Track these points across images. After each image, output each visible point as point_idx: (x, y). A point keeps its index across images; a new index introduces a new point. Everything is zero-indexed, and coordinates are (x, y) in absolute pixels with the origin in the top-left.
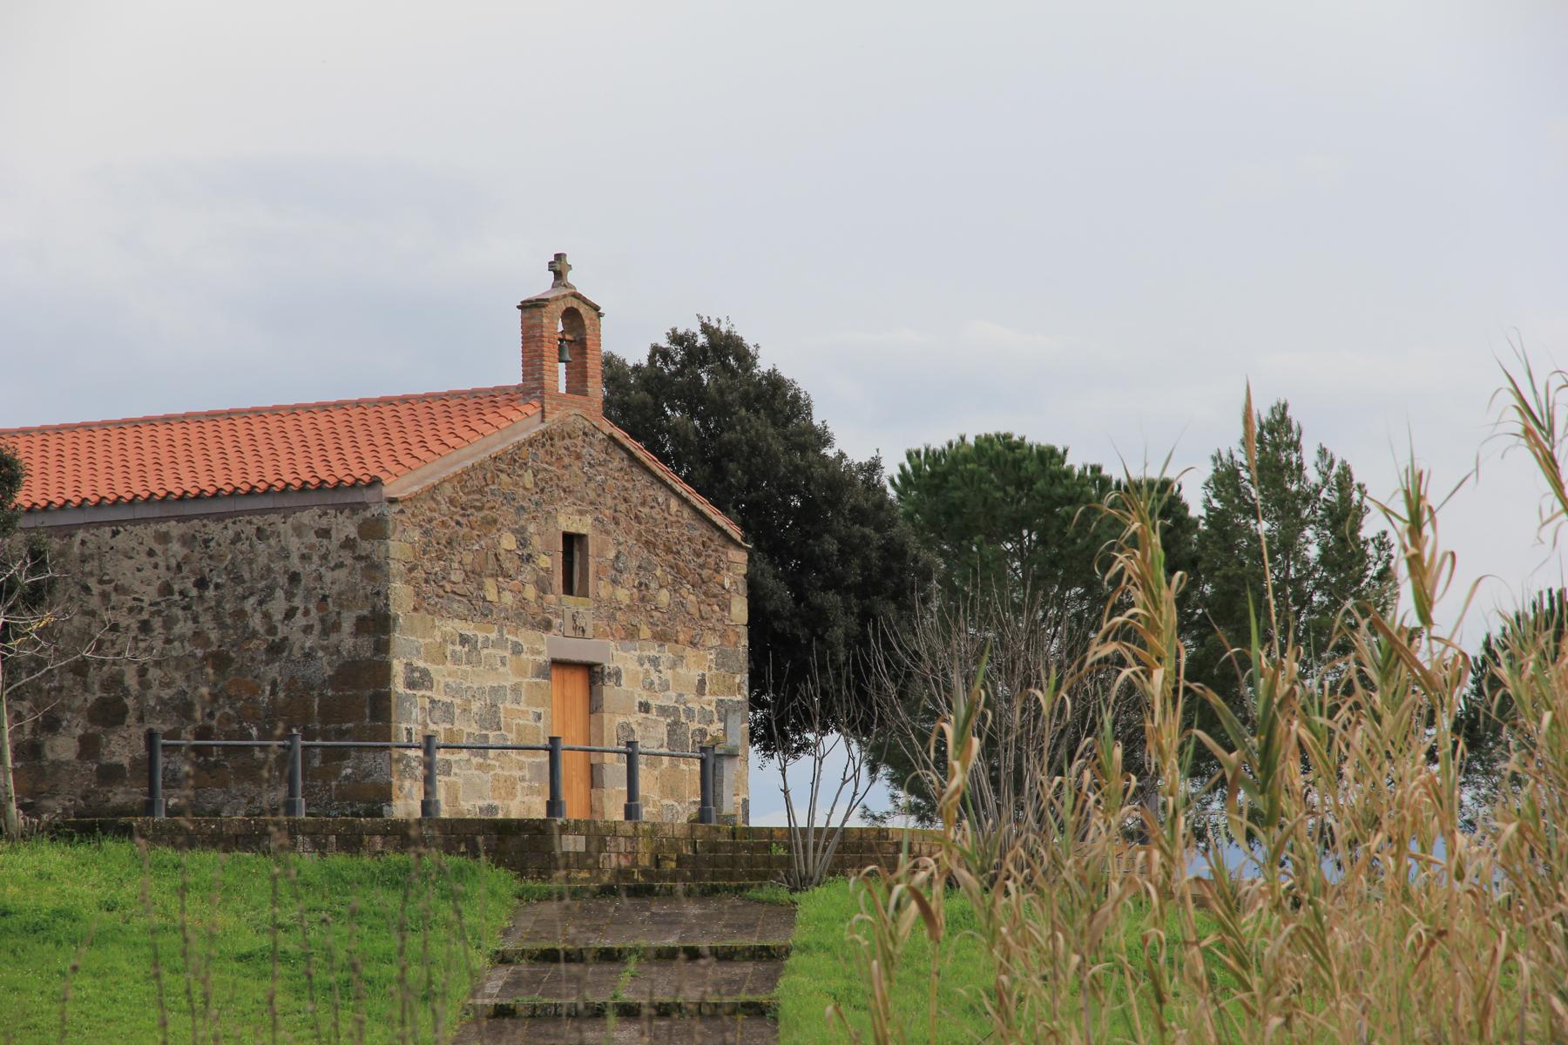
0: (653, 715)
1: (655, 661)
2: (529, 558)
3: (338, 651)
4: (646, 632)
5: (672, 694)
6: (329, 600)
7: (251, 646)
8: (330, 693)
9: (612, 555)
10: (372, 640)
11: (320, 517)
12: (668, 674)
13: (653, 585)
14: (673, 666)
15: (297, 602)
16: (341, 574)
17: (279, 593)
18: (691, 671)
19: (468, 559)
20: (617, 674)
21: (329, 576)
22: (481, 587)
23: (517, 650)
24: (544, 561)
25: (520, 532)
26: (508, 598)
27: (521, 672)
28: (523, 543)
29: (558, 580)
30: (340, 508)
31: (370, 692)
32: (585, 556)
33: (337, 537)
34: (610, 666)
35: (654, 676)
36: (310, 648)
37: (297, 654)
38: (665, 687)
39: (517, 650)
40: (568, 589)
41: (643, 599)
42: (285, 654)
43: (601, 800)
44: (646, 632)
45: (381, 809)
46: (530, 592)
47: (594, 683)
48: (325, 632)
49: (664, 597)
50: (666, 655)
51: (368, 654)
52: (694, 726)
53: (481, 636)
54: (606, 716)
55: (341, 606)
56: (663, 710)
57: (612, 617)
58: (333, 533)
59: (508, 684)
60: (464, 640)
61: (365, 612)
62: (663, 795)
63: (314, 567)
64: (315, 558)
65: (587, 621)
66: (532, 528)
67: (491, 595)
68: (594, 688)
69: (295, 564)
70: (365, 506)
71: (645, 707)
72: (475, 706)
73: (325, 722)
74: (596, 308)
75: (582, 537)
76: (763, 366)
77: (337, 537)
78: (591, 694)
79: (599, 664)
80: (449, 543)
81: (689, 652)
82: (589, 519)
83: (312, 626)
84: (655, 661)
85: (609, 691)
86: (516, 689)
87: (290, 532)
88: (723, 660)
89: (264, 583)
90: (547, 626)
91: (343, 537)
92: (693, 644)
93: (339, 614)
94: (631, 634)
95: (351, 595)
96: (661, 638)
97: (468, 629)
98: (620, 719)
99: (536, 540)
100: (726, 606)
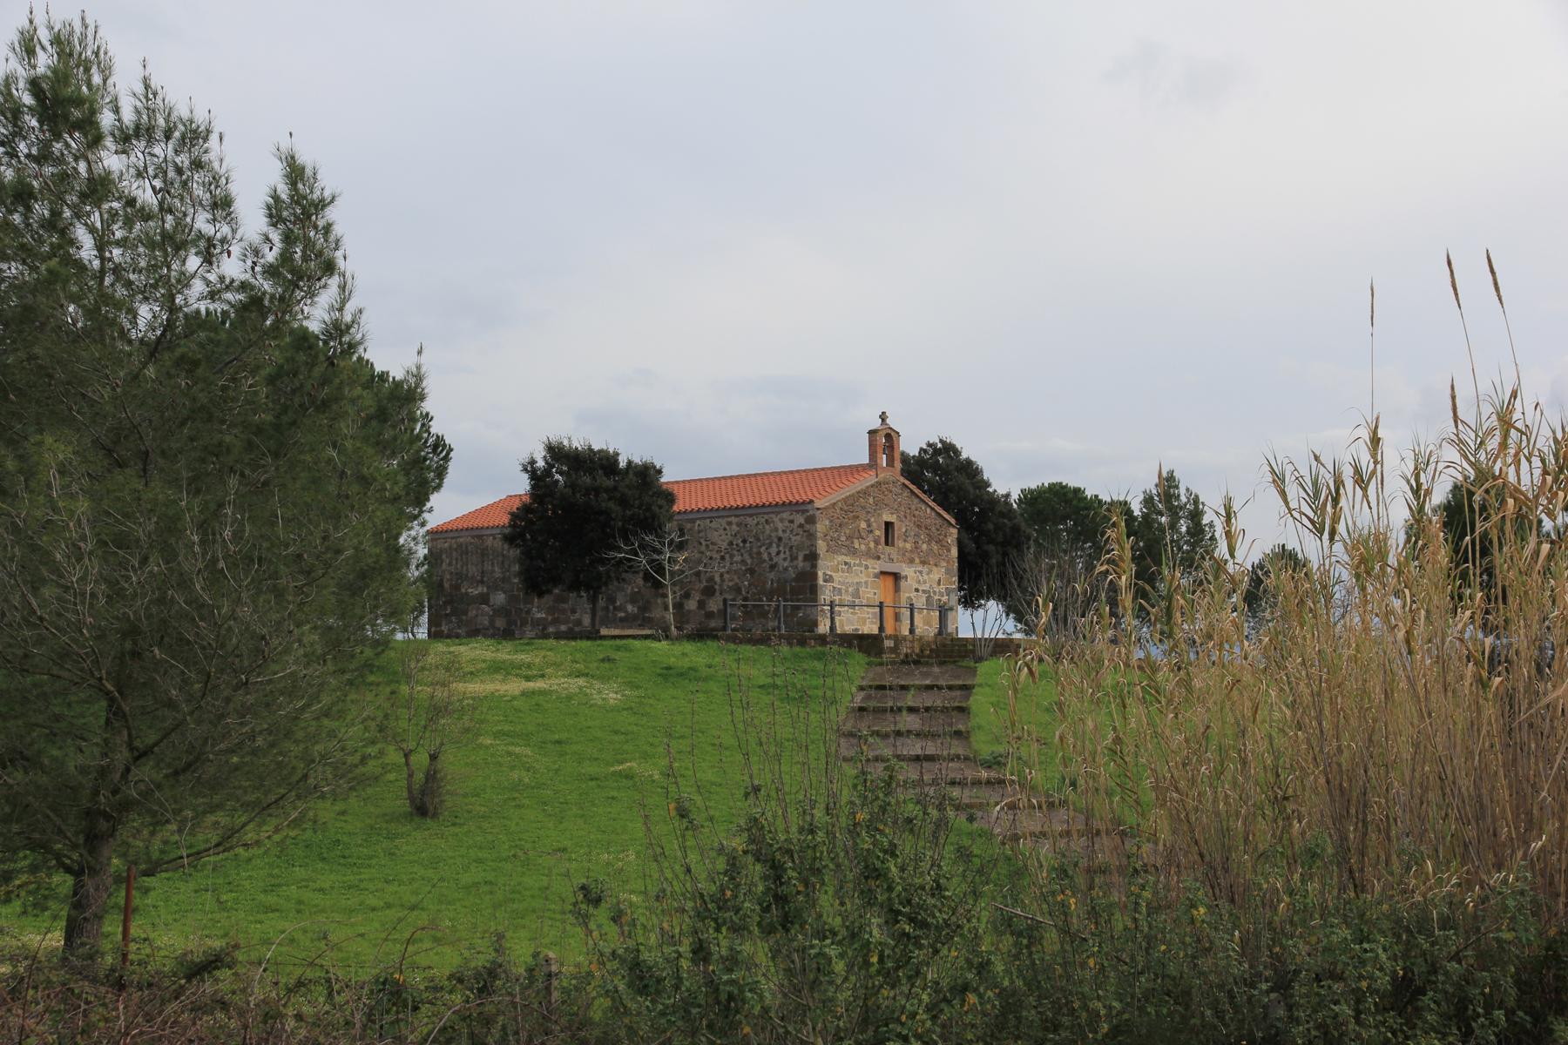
0: (920, 593)
1: (921, 572)
2: (871, 531)
4: (917, 561)
5: (928, 585)
9: (904, 530)
12: (926, 577)
13: (920, 542)
14: (928, 574)
15: (781, 548)
16: (798, 538)
17: (774, 545)
18: (935, 576)
19: (848, 532)
20: (906, 577)
22: (852, 543)
23: (867, 567)
24: (877, 533)
25: (868, 522)
26: (863, 547)
27: (868, 576)
28: (869, 526)
29: (883, 539)
30: (798, 512)
31: (809, 584)
32: (893, 531)
33: (797, 523)
34: (903, 574)
35: (921, 578)
38: (925, 582)
39: (867, 567)
40: (887, 543)
41: (916, 548)
44: (917, 561)
46: (872, 545)
48: (792, 560)
49: (924, 546)
50: (925, 569)
52: (937, 597)
53: (853, 562)
56: (924, 591)
57: (904, 555)
60: (846, 563)
62: (924, 625)
65: (894, 556)
66: (872, 520)
67: (857, 546)
69: (780, 533)
70: (807, 511)
71: (917, 590)
72: (850, 589)
75: (892, 523)
76: (964, 456)
80: (840, 526)
81: (935, 568)
82: (895, 516)
84: (921, 572)
85: (903, 583)
86: (866, 582)
88: (948, 572)
90: (879, 558)
92: (936, 565)
94: (912, 561)
96: (923, 563)
97: (848, 559)
98: (907, 595)
99: (874, 524)
100: (949, 550)
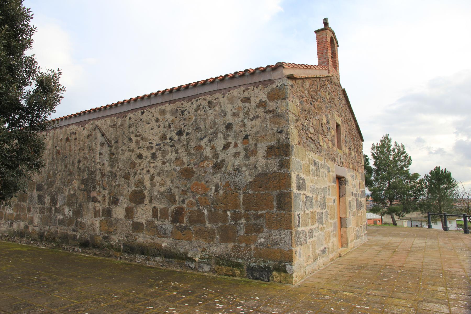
3: (255, 167)
6: (250, 137)
7: (205, 165)
8: (250, 192)
10: (278, 160)
11: (244, 91)
15: (231, 139)
16: (257, 122)
17: (220, 136)
21: (249, 124)
30: (256, 85)
33: (254, 101)
36: (238, 166)
37: (230, 169)
42: (223, 169)
43: (346, 232)
45: (285, 266)
47: (341, 185)
48: (247, 157)
51: (275, 169)
54: (347, 198)
55: (257, 141)
58: (252, 99)
59: (327, 186)
61: (273, 143)
63: (240, 119)
64: (241, 114)
68: (341, 187)
69: (229, 118)
70: (271, 81)
73: (247, 209)
74: (337, 43)
77: (254, 101)
78: (339, 189)
79: (344, 177)
83: (239, 153)
87: (227, 102)
89: (212, 130)
91: (258, 101)
93: (256, 145)
95: (263, 134)
